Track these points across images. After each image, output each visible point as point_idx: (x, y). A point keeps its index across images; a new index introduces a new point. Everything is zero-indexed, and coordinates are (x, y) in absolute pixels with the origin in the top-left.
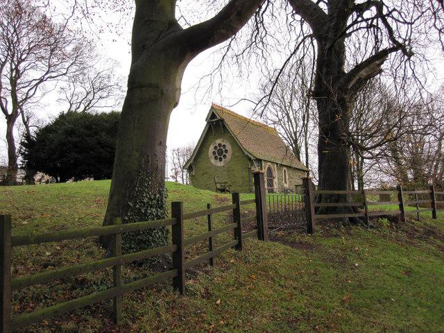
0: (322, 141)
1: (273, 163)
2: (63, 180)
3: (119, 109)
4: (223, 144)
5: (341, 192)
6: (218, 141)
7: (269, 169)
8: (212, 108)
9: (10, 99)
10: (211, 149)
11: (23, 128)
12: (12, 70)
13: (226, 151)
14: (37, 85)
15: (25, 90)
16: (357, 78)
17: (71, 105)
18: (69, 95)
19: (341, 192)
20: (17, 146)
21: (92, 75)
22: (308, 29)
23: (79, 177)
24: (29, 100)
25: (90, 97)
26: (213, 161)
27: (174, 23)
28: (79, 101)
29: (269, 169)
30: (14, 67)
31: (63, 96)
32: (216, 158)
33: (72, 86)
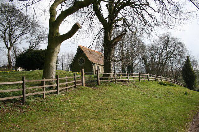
0: (105, 61)
1: (99, 64)
2: (29, 70)
3: (47, 49)
4: (82, 58)
5: (109, 74)
6: (81, 57)
7: (98, 67)
8: (79, 46)
9: (9, 42)
10: (79, 60)
11: (13, 51)
12: (10, 32)
13: (84, 61)
14: (18, 37)
15: (15, 38)
16: (114, 41)
17: (31, 44)
18: (30, 40)
19: (109, 74)
20: (12, 58)
21: (38, 33)
22: (102, 26)
23: (34, 69)
24: (16, 42)
25: (38, 41)
26: (79, 64)
27: (58, 33)
28: (34, 42)
29: (98, 67)
30: (10, 30)
31: (28, 40)
32: (80, 63)
33: (31, 37)
